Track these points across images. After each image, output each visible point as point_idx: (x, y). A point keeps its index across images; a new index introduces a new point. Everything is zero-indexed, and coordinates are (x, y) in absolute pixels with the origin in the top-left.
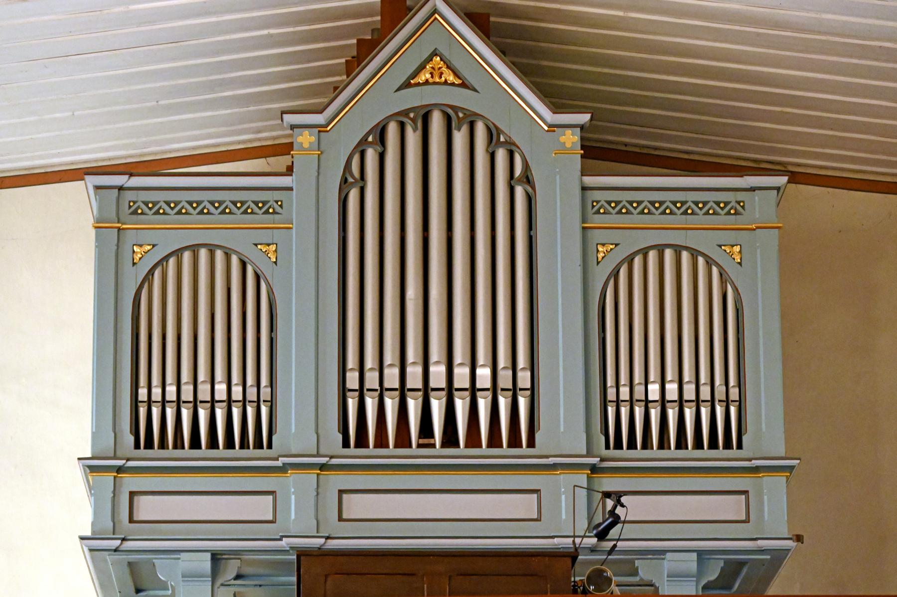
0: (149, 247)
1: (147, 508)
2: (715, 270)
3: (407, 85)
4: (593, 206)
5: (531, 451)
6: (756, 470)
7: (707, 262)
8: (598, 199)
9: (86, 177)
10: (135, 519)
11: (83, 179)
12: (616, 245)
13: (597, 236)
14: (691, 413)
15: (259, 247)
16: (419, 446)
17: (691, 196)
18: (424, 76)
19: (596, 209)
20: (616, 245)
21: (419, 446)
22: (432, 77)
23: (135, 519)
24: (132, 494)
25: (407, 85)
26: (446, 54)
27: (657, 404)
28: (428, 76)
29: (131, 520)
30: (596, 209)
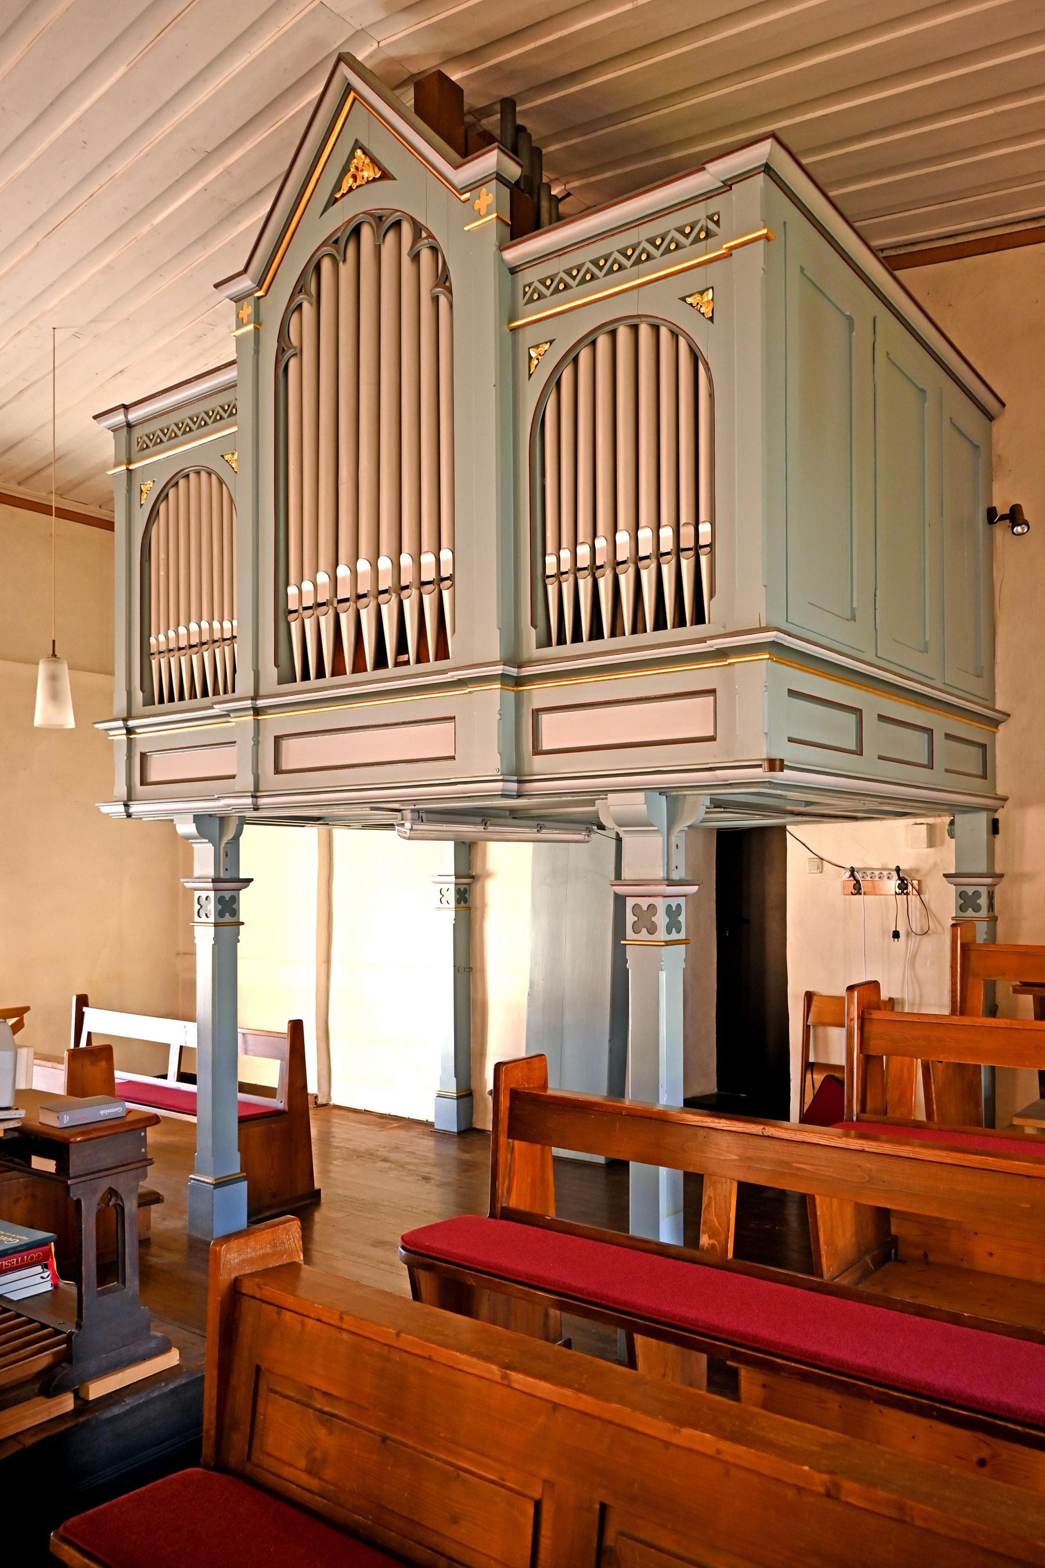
0: (546, 347)
1: (295, 754)
2: (682, 342)
3: (333, 201)
4: (525, 293)
5: (443, 664)
6: (722, 654)
7: (672, 332)
8: (529, 282)
9: (707, 166)
10: (284, 767)
11: (704, 169)
12: (551, 342)
13: (528, 337)
14: (327, 621)
15: (689, 300)
16: (397, 664)
17: (177, 417)
18: (348, 182)
19: (528, 295)
20: (551, 342)
21: (397, 664)
22: (355, 181)
23: (284, 767)
24: (278, 739)
25: (333, 201)
26: (365, 144)
27: (586, 572)
28: (351, 180)
29: (278, 770)
30: (528, 295)
